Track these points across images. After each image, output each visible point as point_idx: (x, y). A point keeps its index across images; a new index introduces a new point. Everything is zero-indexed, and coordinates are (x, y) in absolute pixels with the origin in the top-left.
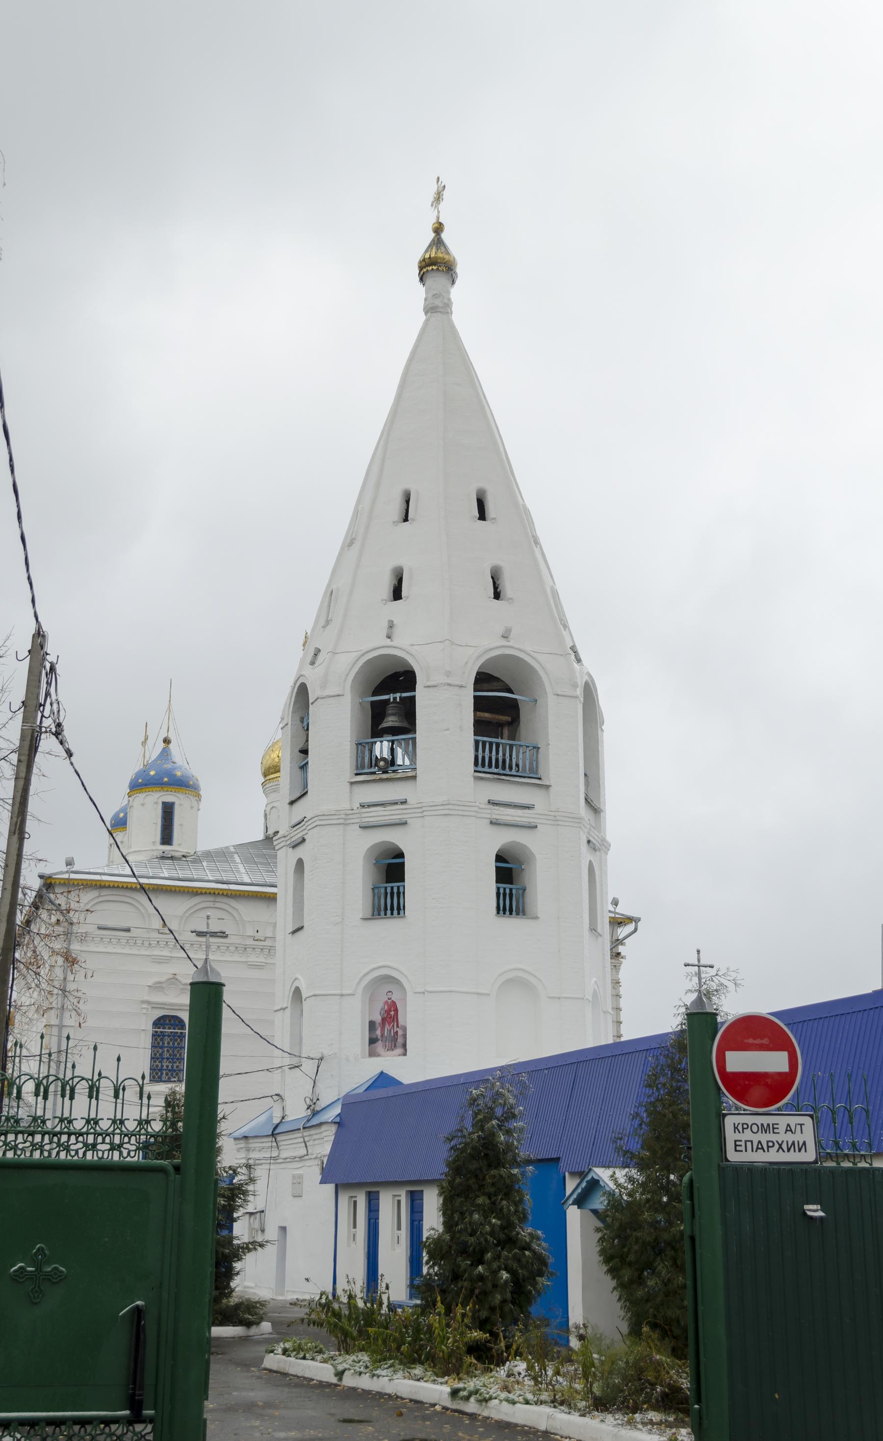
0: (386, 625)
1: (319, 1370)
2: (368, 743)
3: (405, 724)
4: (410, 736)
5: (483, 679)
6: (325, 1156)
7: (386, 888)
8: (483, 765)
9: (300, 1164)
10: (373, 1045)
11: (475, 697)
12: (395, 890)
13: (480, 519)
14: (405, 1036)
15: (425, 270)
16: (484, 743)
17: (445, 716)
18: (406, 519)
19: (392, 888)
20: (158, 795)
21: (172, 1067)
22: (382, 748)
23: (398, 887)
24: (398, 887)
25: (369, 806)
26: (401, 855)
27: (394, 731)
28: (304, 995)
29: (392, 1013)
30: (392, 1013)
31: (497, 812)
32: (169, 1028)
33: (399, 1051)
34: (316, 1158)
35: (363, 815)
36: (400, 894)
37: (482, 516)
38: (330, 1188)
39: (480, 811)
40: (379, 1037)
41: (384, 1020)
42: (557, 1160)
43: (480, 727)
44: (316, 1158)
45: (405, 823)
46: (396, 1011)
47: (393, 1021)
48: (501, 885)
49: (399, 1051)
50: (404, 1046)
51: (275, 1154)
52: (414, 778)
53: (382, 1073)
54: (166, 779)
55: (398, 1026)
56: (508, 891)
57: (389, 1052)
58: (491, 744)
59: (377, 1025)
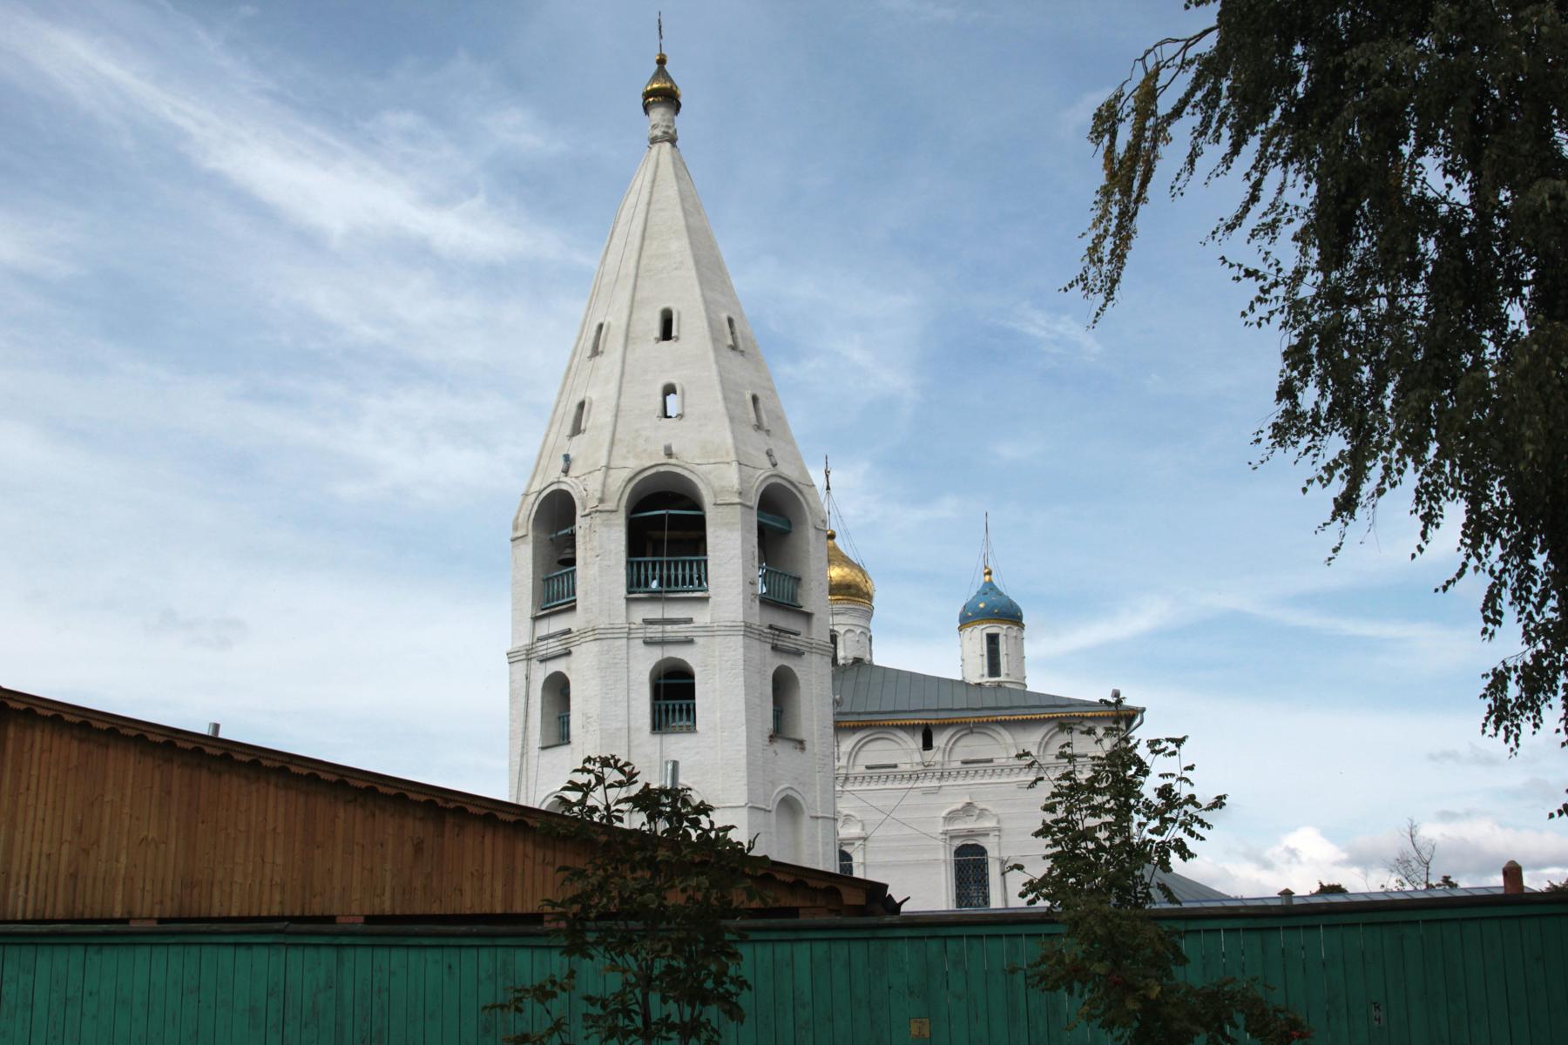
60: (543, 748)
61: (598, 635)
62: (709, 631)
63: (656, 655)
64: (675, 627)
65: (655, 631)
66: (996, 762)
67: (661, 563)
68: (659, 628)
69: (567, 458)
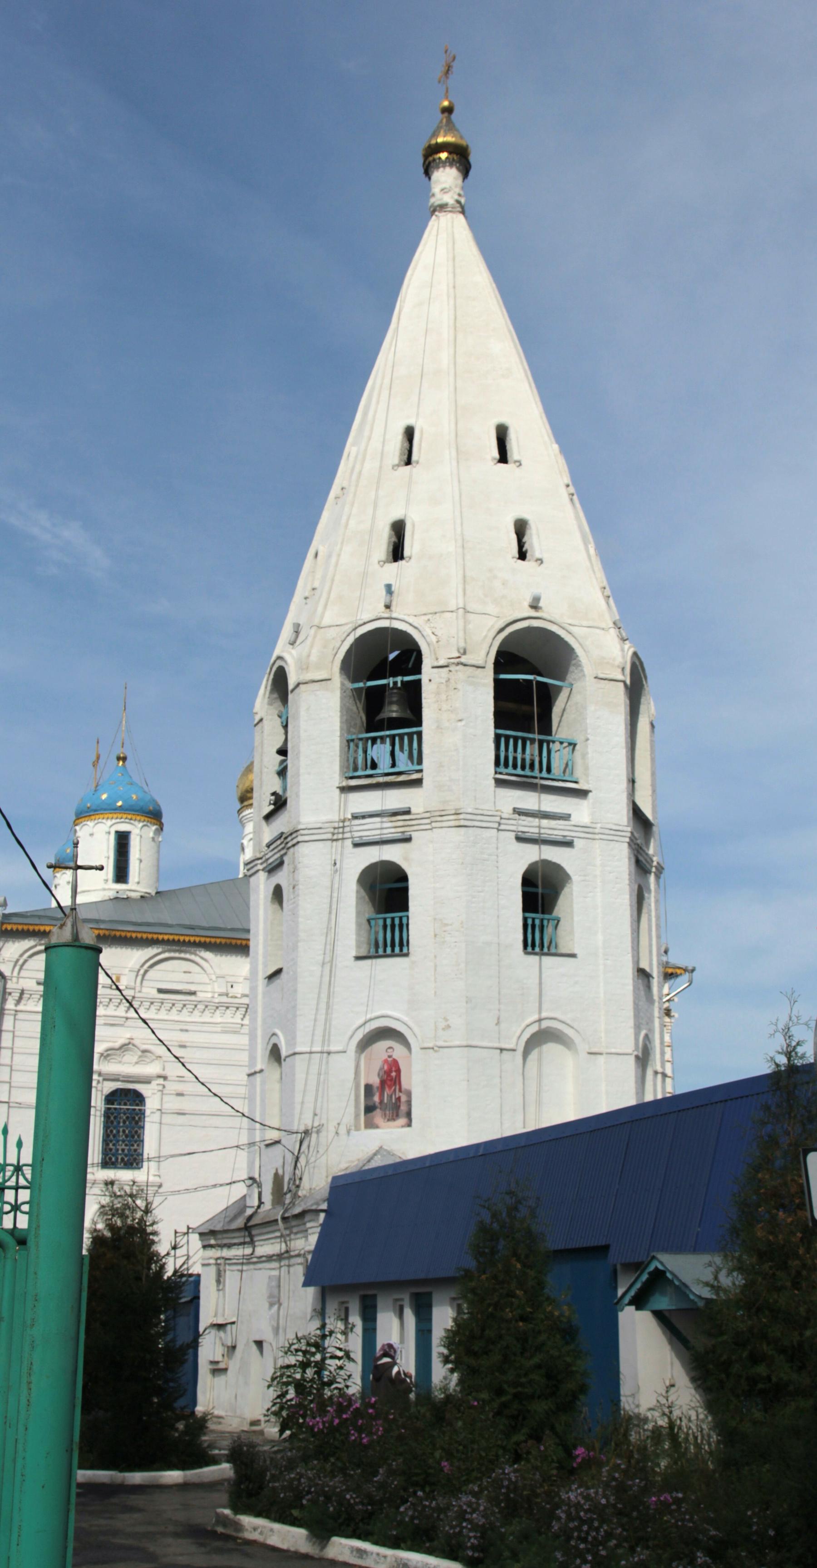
0: (384, 592)
1: (653, 905)
2: (361, 739)
3: (408, 714)
4: (414, 729)
5: (507, 659)
6: (309, 1252)
7: (385, 920)
8: (506, 765)
10: (370, 1114)
12: (397, 922)
14: (409, 1103)
15: (431, 159)
16: (507, 738)
17: (458, 712)
18: (408, 462)
19: (393, 919)
20: (109, 823)
21: (129, 1150)
22: (380, 752)
23: (401, 918)
24: (401, 918)
25: (364, 817)
26: (404, 878)
27: (395, 723)
28: (284, 1053)
29: (394, 1074)
30: (394, 1074)
32: (125, 1104)
33: (402, 1121)
35: (355, 828)
36: (403, 926)
37: (503, 458)
38: (311, 1292)
40: (377, 1104)
41: (383, 1083)
42: (603, 1250)
43: (502, 718)
46: (398, 1071)
47: (395, 1084)
48: (527, 915)
49: (402, 1121)
50: (409, 1115)
53: (381, 1147)
54: (120, 803)
55: (400, 1090)
56: (537, 922)
57: (391, 1123)
58: (516, 739)
59: (375, 1090)
60: (358, 958)
61: (462, 820)
62: (588, 831)
63: (531, 854)
64: (553, 823)
65: (530, 826)
66: (201, 996)
67: (532, 741)
68: (536, 821)
69: (389, 588)
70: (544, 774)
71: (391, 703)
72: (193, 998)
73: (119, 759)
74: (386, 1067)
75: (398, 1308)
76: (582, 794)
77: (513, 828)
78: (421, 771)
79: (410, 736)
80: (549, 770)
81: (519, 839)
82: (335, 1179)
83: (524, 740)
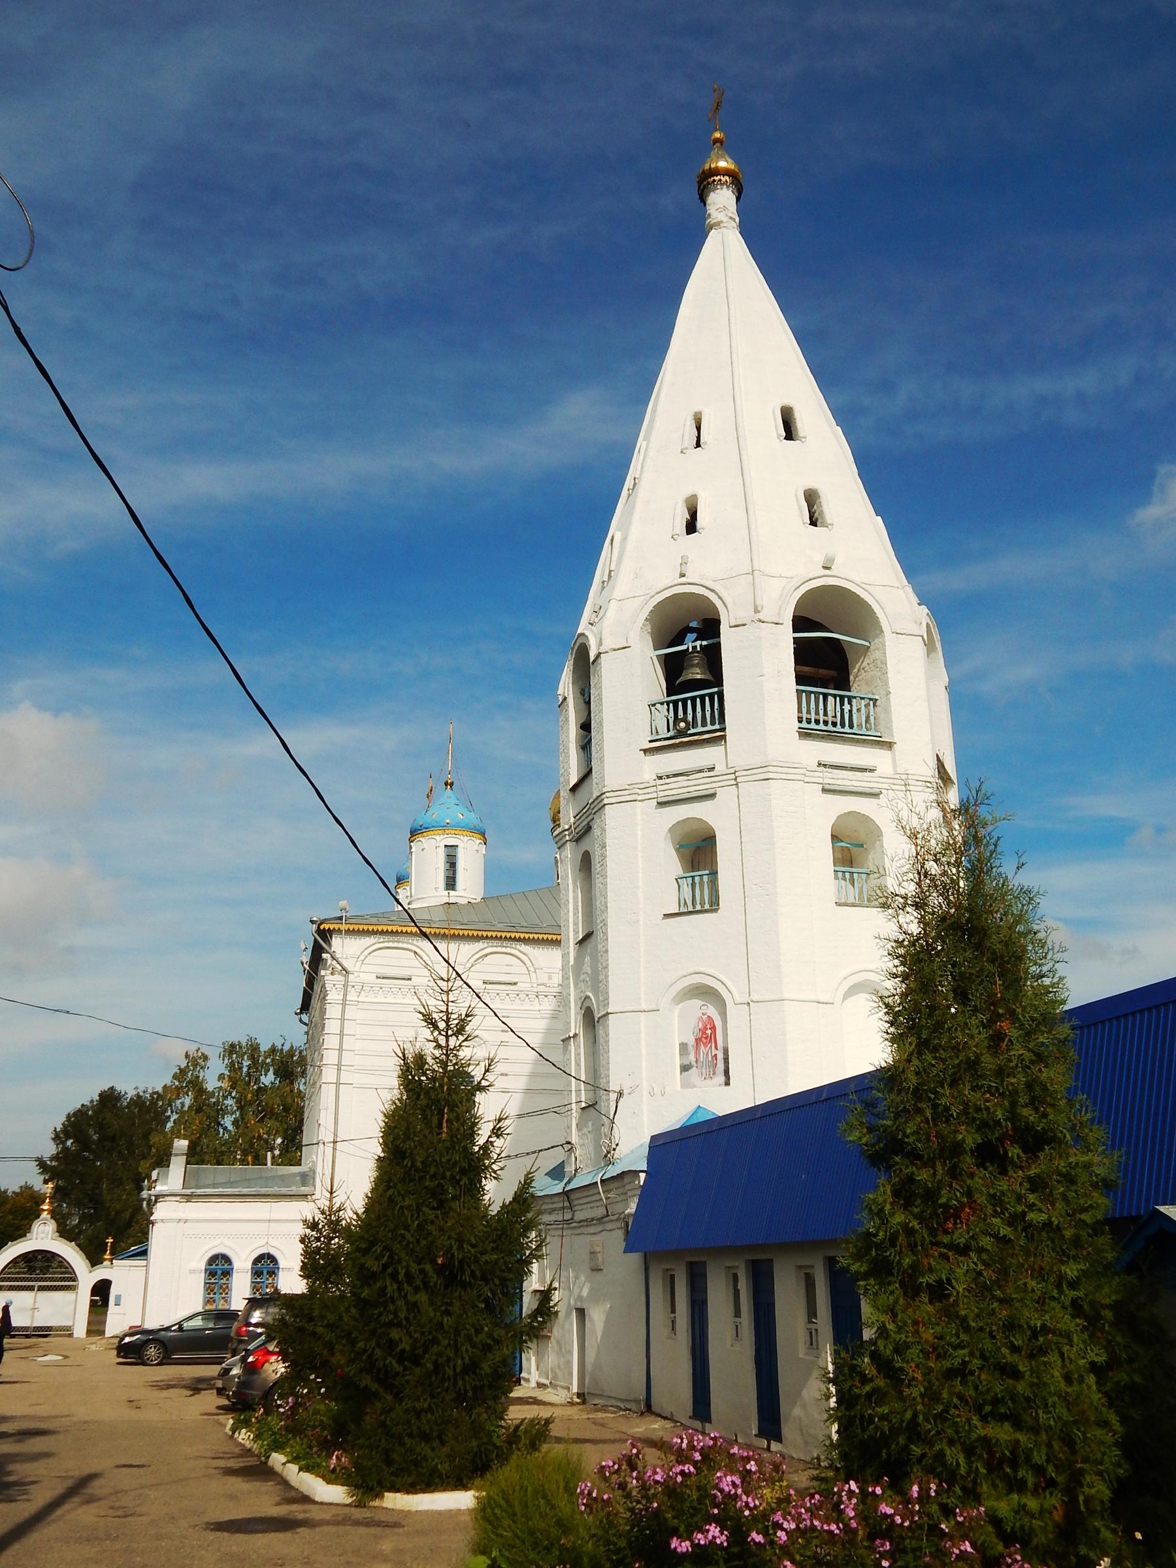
3: (709, 677)
4: (716, 690)
9: (600, 1228)
10: (685, 1074)
11: (796, 641)
13: (787, 438)
16: (809, 693)
17: (760, 666)
30: (709, 1032)
31: (830, 775)
34: (618, 1220)
37: (790, 434)
38: (635, 1259)
39: (808, 773)
40: (693, 1063)
41: (698, 1041)
44: (618, 1220)
45: (712, 796)
51: (568, 1216)
52: (724, 737)
57: (708, 1082)
70: (847, 729)
71: (693, 666)
72: (514, 987)
73: (446, 784)
74: (700, 1025)
75: (731, 1278)
76: (889, 745)
77: (820, 781)
78: (723, 730)
79: (711, 696)
80: (851, 726)
81: (824, 790)
82: (654, 1138)
83: (825, 696)
